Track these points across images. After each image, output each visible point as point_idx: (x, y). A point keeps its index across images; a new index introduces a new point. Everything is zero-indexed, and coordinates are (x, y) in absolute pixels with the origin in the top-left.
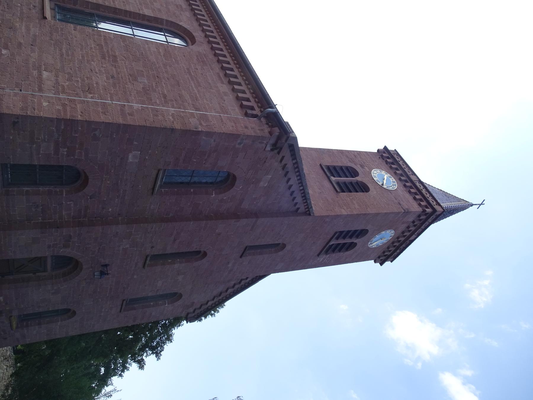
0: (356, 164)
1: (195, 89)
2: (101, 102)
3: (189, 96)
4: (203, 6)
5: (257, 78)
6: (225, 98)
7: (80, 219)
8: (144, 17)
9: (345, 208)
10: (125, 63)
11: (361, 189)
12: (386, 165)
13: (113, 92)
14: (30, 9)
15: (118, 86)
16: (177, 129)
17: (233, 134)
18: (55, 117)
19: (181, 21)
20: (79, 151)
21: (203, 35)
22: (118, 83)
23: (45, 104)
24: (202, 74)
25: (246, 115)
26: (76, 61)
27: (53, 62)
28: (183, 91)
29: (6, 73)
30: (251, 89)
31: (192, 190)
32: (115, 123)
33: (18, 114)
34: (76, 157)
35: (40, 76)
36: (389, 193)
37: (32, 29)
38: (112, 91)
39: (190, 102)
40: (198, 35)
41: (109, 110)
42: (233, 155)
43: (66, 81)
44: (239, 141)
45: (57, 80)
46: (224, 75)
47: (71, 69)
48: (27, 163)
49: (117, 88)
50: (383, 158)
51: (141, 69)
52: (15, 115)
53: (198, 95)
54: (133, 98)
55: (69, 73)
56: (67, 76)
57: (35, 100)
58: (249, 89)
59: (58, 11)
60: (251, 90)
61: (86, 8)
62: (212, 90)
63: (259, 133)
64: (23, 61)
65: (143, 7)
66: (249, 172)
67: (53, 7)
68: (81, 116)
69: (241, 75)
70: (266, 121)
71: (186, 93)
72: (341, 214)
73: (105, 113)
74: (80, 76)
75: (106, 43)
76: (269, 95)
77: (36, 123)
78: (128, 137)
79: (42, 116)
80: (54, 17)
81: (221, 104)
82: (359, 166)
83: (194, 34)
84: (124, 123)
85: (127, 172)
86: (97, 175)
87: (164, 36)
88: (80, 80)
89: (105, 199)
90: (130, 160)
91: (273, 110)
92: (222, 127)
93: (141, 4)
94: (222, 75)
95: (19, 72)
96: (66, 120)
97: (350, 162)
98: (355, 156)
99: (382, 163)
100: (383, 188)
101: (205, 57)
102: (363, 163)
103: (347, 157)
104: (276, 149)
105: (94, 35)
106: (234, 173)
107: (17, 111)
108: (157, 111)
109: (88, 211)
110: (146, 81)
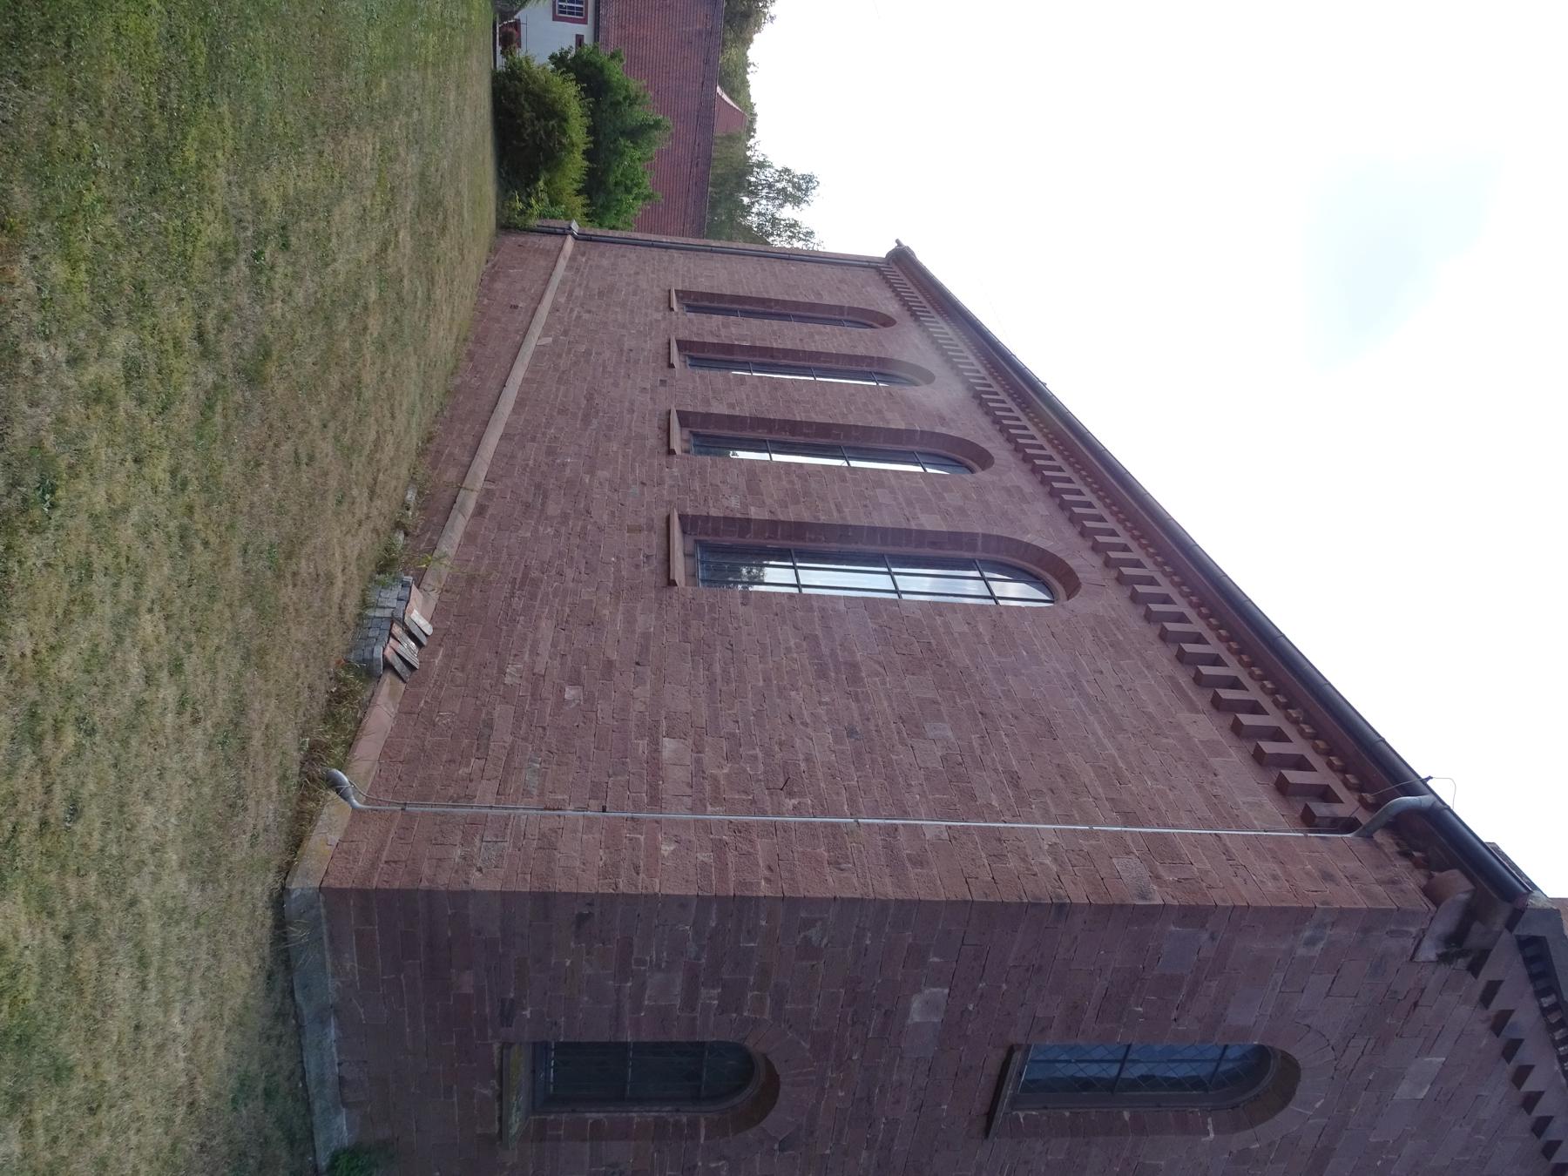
1: (1106, 741)
2: (826, 825)
3: (1090, 769)
4: (1083, 478)
6: (1215, 762)
8: (922, 536)
10: (884, 683)
14: (637, 566)
16: (1077, 904)
17: (1285, 910)
18: (693, 891)
19: (1026, 532)
20: (756, 993)
21: (1097, 561)
25: (1309, 820)
26: (750, 696)
27: (690, 707)
28: (1070, 755)
31: (1126, 1115)
32: (870, 900)
33: (593, 891)
34: (745, 1014)
37: (641, 619)
39: (1100, 790)
40: (1084, 563)
41: (849, 853)
42: (1284, 983)
43: (722, 762)
44: (1307, 934)
45: (698, 761)
46: (1192, 682)
47: (737, 722)
48: (605, 1038)
51: (930, 695)
52: (584, 895)
53: (1121, 764)
54: (918, 797)
56: (724, 744)
58: (1295, 722)
59: (702, 557)
60: (1303, 726)
61: (770, 538)
62: (1165, 740)
63: (1385, 899)
65: (918, 511)
66: (1350, 1045)
67: (690, 548)
68: (768, 880)
69: (1251, 675)
70: (1398, 844)
73: (840, 864)
74: (761, 740)
75: (827, 628)
76: (1387, 740)
78: (910, 940)
79: (657, 890)
80: (692, 576)
81: (1208, 787)
83: (1071, 563)
84: (901, 895)
85: (901, 1058)
86: (805, 1070)
87: (983, 582)
88: (760, 755)
89: (828, 1152)
90: (915, 1017)
91: (1420, 801)
93: (910, 503)
94: (1184, 680)
95: (603, 750)
96: (722, 900)
101: (1118, 629)
104: (1463, 954)
105: (795, 609)
106: (1283, 1049)
107: (591, 884)
108: (1000, 840)
110: (950, 734)
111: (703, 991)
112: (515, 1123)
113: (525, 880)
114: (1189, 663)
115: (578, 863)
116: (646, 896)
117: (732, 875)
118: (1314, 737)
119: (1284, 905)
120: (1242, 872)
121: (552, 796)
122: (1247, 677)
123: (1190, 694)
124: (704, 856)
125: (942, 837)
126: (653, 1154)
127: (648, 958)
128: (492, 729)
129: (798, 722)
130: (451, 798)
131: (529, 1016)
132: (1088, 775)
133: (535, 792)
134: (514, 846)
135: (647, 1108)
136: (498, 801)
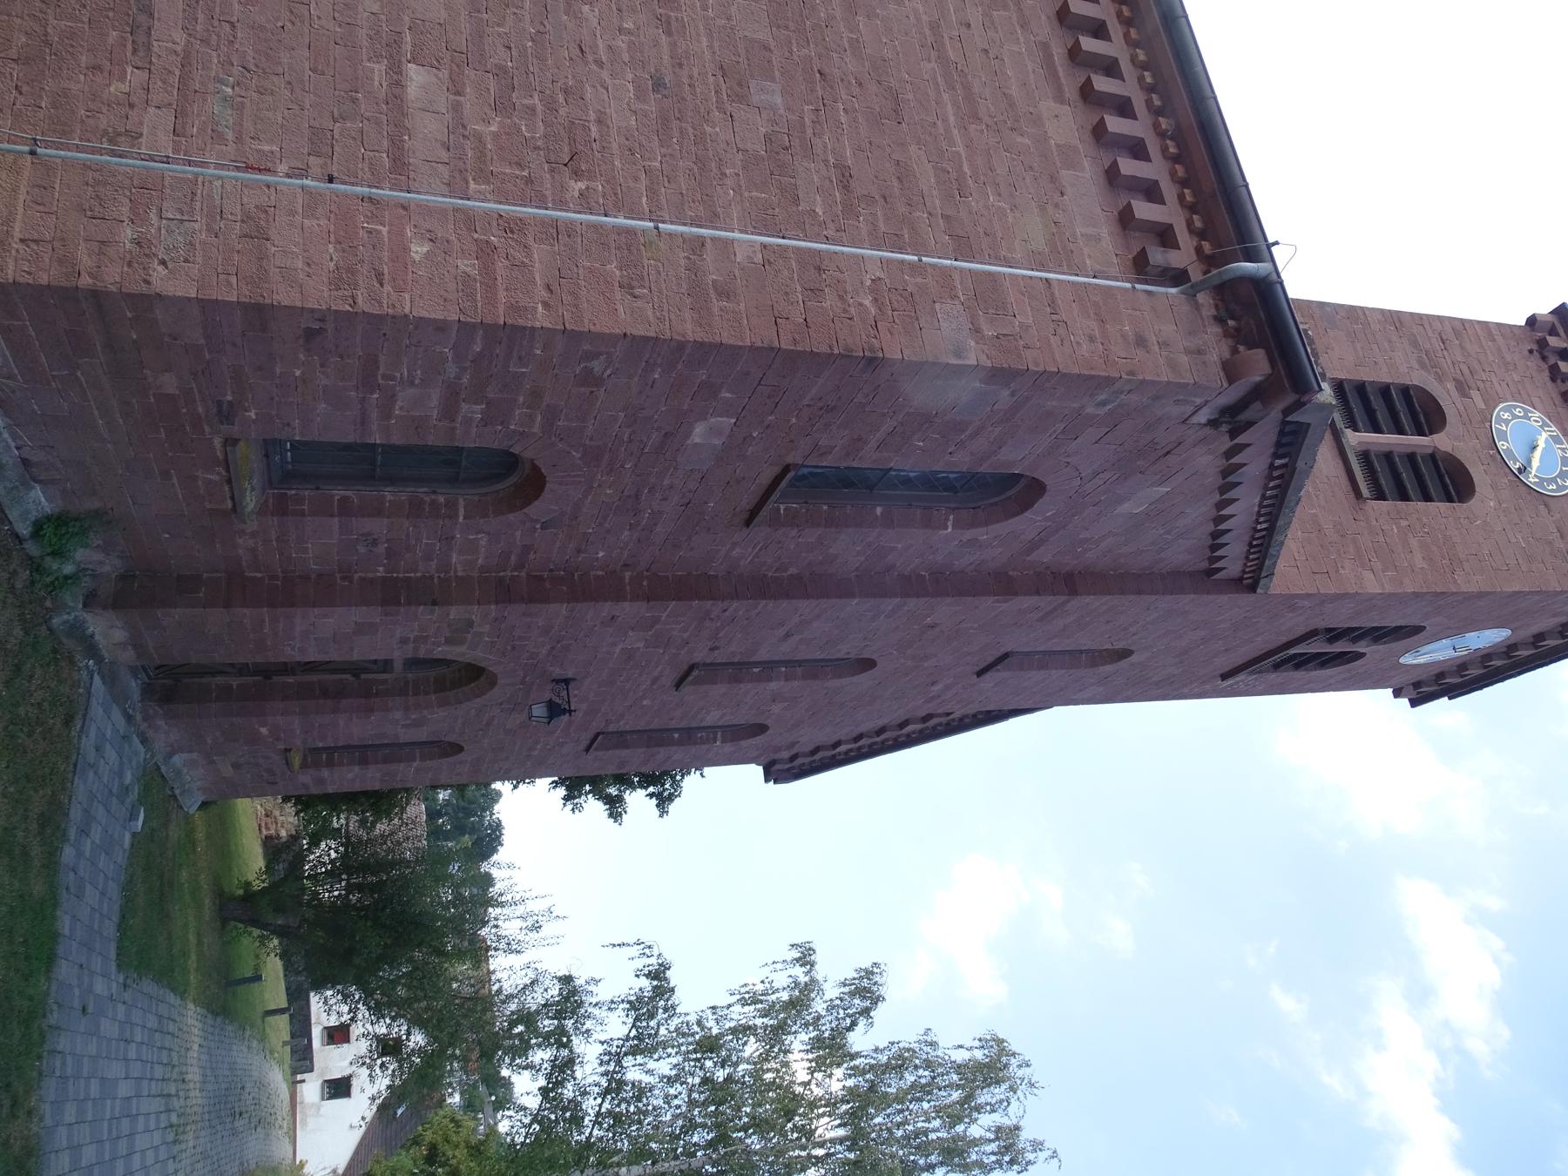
0: (1440, 379)
5: (1209, 93)
6: (1066, 175)
7: (502, 574)
9: (1378, 565)
11: (1444, 486)
12: (1550, 384)
13: (658, 164)
15: (676, 133)
22: (677, 115)
23: (417, 252)
24: (986, 51)
25: (1141, 267)
28: (913, 148)
29: (275, 78)
30: (1172, 139)
34: (512, 427)
35: (397, 91)
36: (1542, 507)
38: (655, 159)
39: (937, 202)
41: (645, 274)
44: (1102, 397)
45: (456, 108)
47: (510, 48)
48: (350, 439)
49: (675, 140)
50: (1546, 354)
51: (760, 36)
52: (312, 311)
53: (966, 168)
55: (500, 72)
57: (379, 232)
58: (1162, 135)
62: (1019, 139)
64: (337, 15)
68: (546, 305)
70: (1216, 306)
71: (924, 158)
72: (1360, 591)
73: (633, 288)
77: (385, 334)
78: (704, 377)
79: (407, 310)
82: (1450, 386)
84: (701, 336)
85: (675, 469)
88: (539, 108)
92: (1055, 341)
94: (1059, 52)
97: (1422, 365)
98: (1442, 339)
99: (1534, 374)
100: (1524, 488)
102: (1466, 371)
103: (1415, 344)
107: (319, 295)
109: (532, 556)
110: (779, 100)
111: (464, 407)
112: (251, 502)
113: (229, 283)
114: (1070, 28)
115: (300, 264)
116: (394, 317)
117: (502, 295)
118: (1176, 159)
119: (1093, 373)
120: (1061, 331)
121: (256, 145)
122: (1143, 104)
123: (1061, 74)
124: (468, 265)
125: (755, 260)
126: (408, 528)
127: (398, 375)
128: (151, 15)
129: (590, 58)
130: (105, 132)
131: (254, 417)
132: (927, 180)
133: (230, 136)
134: (209, 229)
135: (401, 489)
136: (176, 151)
